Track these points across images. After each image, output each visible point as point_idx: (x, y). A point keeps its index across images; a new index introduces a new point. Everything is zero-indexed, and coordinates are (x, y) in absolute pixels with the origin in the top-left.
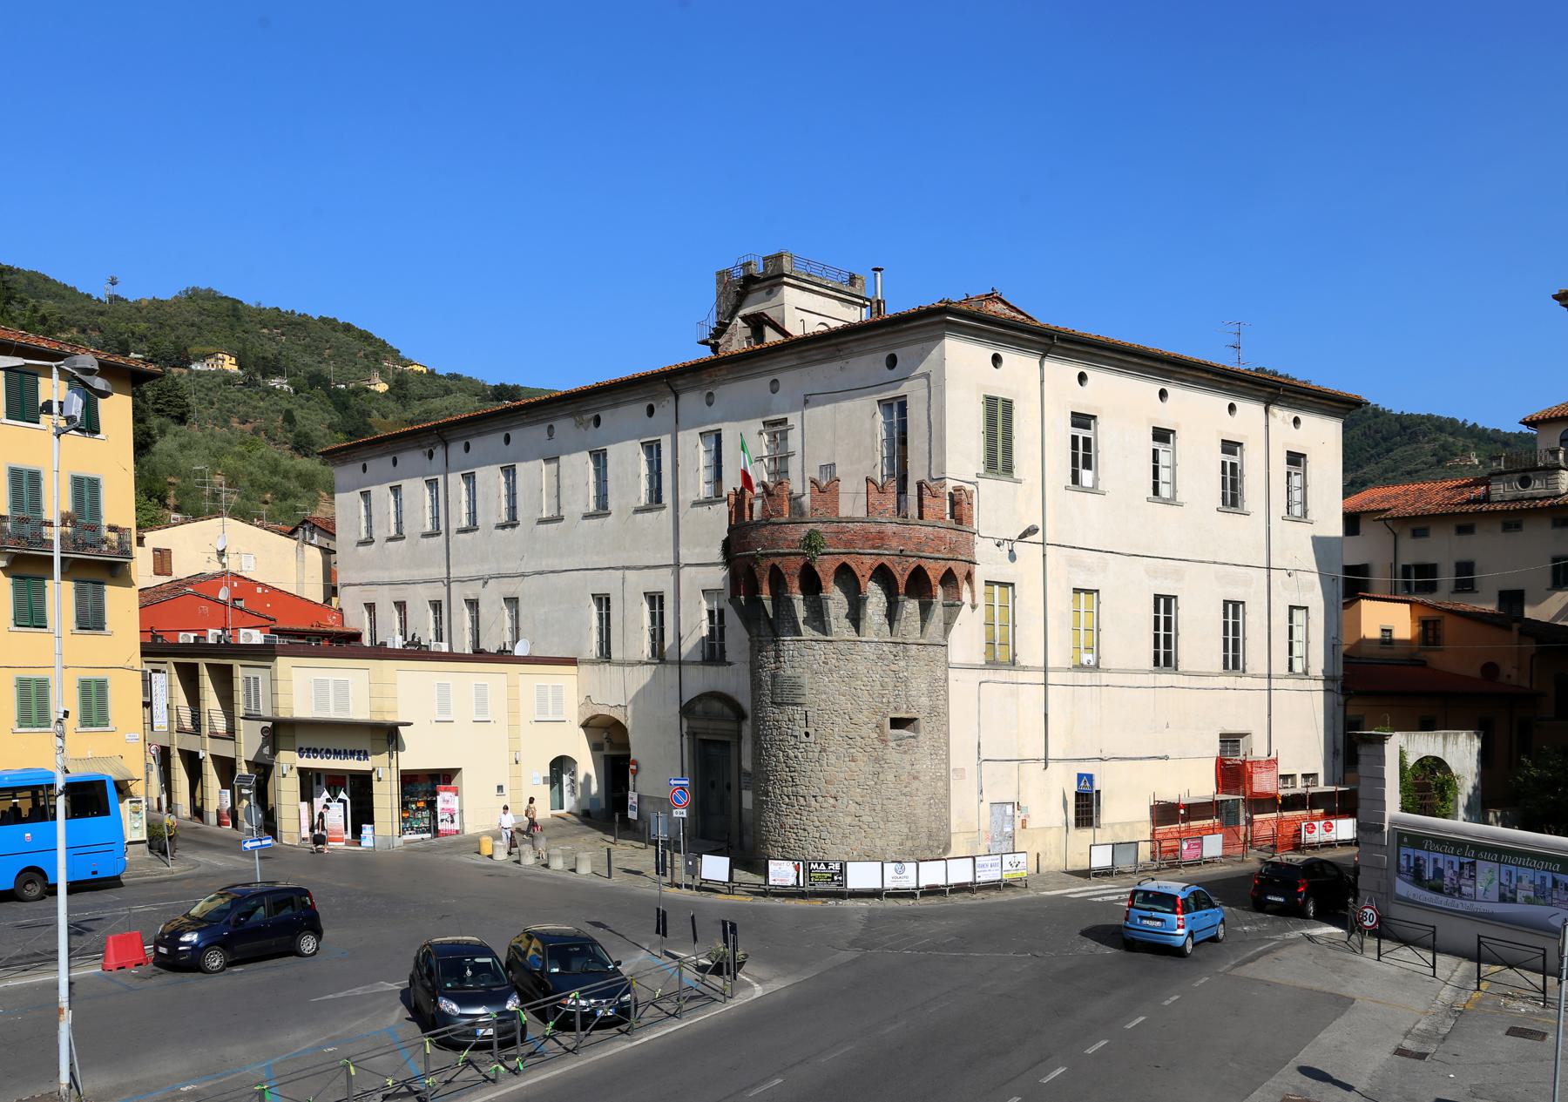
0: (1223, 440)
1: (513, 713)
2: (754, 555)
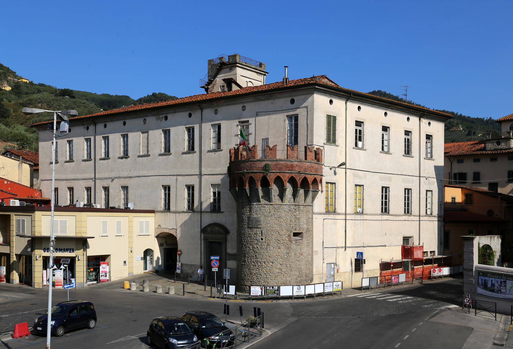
0: (405, 131)
1: (130, 232)
2: (243, 173)
